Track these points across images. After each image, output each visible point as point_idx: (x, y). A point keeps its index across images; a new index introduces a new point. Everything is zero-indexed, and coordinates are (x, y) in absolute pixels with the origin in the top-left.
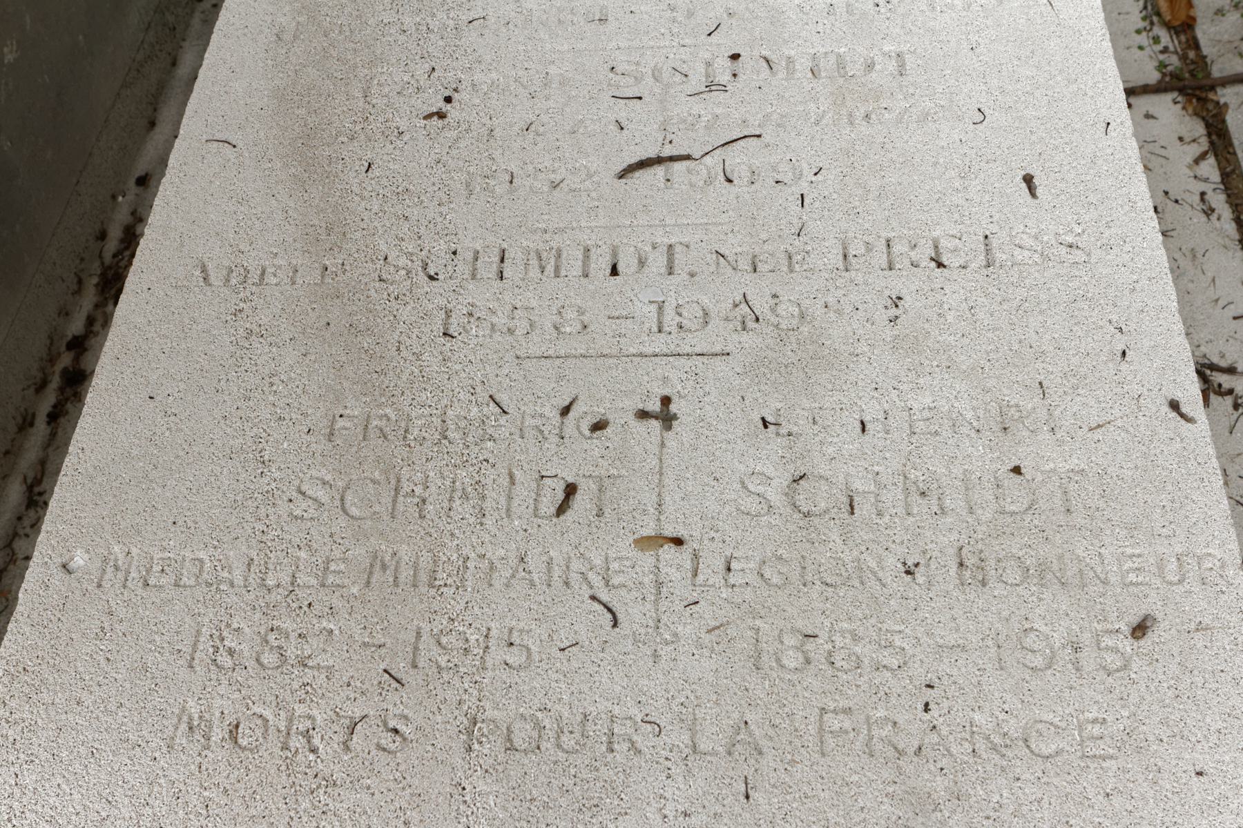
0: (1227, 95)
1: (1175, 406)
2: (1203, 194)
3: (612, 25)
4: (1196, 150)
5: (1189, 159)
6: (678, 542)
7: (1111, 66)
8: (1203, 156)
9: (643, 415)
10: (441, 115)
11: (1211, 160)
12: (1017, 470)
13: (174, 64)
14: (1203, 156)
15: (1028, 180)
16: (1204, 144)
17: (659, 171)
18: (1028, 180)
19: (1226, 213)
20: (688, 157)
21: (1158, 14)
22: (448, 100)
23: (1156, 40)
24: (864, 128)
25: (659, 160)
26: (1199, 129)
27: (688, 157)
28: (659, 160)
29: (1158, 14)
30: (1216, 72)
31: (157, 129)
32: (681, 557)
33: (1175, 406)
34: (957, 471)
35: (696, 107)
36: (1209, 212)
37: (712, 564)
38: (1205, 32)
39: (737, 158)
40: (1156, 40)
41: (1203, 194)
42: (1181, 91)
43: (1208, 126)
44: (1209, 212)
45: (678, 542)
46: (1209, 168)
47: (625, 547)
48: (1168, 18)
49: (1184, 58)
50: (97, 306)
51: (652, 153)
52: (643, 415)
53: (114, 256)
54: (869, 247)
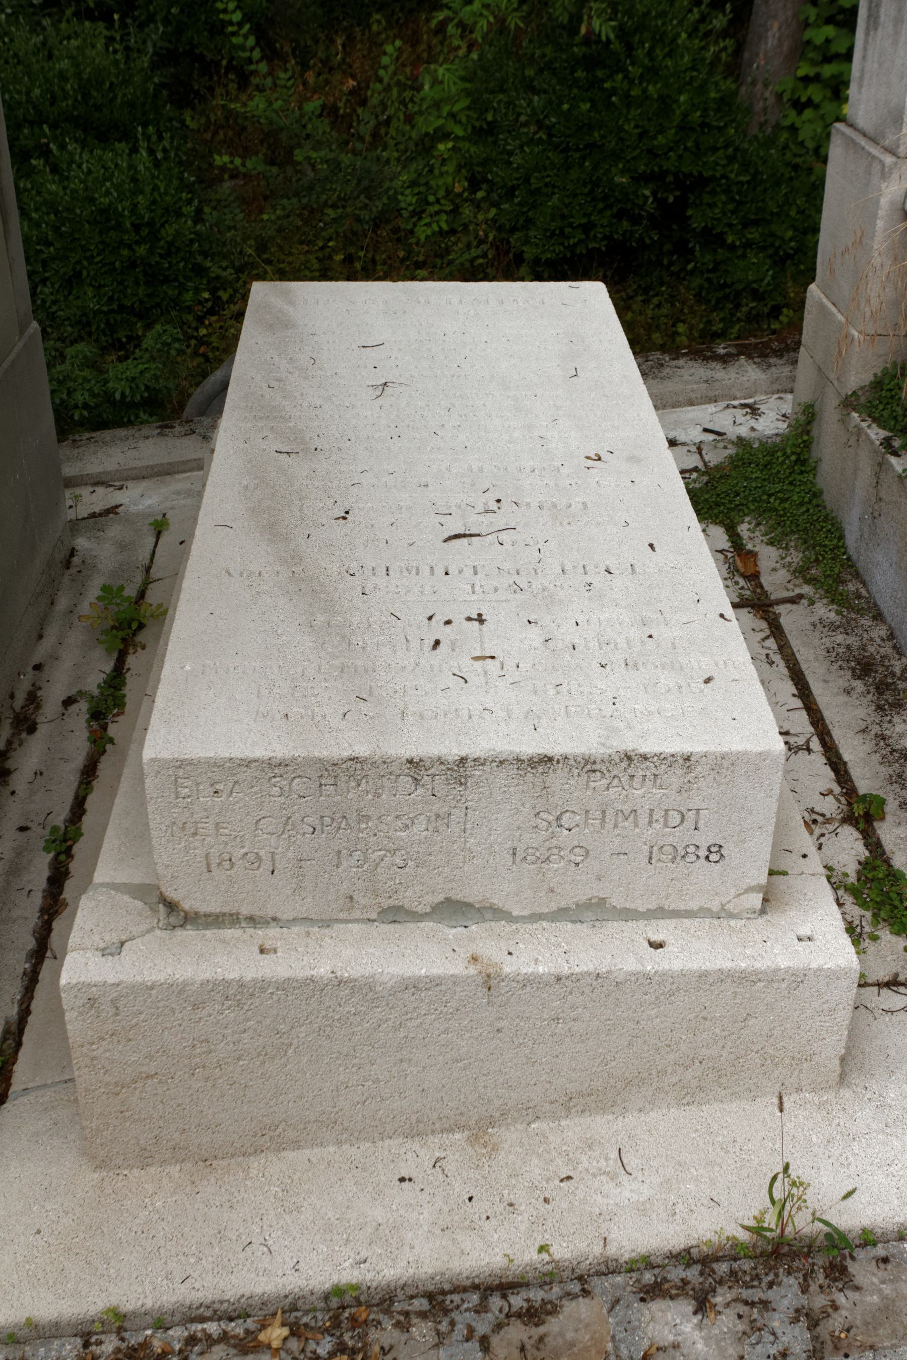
0: (780, 609)
1: (722, 616)
2: (767, 655)
3: (430, 488)
4: (763, 635)
5: (759, 639)
6: (493, 657)
7: (674, 465)
8: (767, 638)
9: (469, 619)
10: (344, 518)
11: (772, 640)
12: (650, 636)
13: (52, 603)
14: (767, 638)
15: (651, 546)
16: (767, 632)
17: (465, 541)
18: (651, 546)
19: (782, 664)
20: (479, 535)
21: (737, 571)
22: (347, 513)
23: (737, 583)
24: (568, 527)
25: (465, 536)
26: (764, 625)
27: (479, 535)
28: (465, 536)
29: (737, 571)
30: (773, 597)
31: (44, 640)
32: (496, 663)
33: (722, 616)
34: (623, 637)
35: (481, 518)
36: (771, 663)
37: (510, 664)
38: (765, 580)
39: (503, 536)
40: (737, 583)
41: (767, 655)
42: (752, 607)
43: (769, 624)
44: (771, 663)
45: (493, 657)
46: (771, 643)
47: (466, 661)
48: (742, 570)
49: (754, 592)
50: (13, 735)
51: (462, 532)
52: (469, 619)
53: (22, 708)
54: (574, 567)
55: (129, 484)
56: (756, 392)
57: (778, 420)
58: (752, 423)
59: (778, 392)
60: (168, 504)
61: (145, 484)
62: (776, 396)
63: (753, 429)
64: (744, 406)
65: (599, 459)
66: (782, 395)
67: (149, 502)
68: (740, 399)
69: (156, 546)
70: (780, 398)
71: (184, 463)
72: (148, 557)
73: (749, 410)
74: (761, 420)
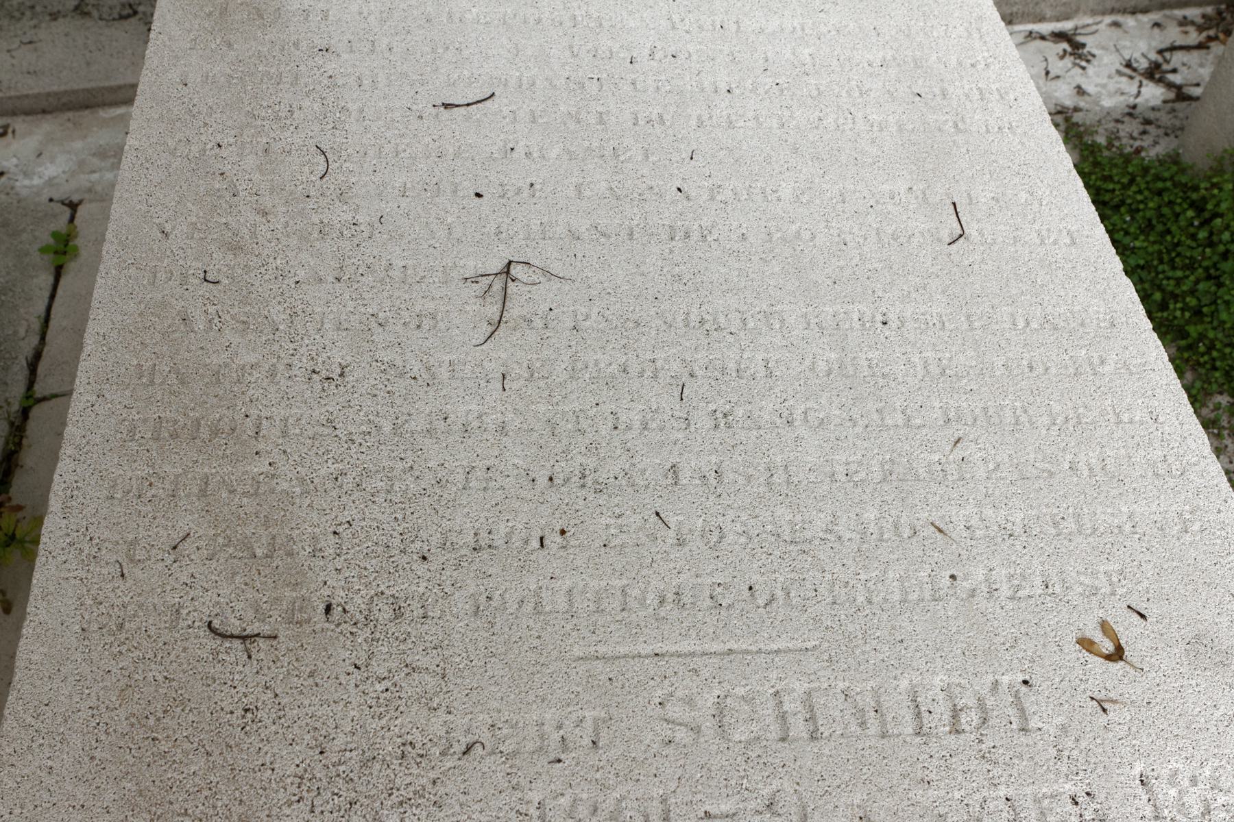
55: (19, 124)
56: (1077, 11)
57: (1119, 73)
58: (1077, 77)
59: (1113, 11)
60: (84, 180)
61: (47, 126)
62: (1108, 19)
63: (1080, 91)
64: (1059, 36)
65: (1118, 654)
66: (1119, 18)
67: (50, 170)
68: (1050, 20)
69: (52, 297)
70: (1116, 24)
71: (112, 90)
72: (36, 326)
73: (1065, 46)
74: (1091, 70)
